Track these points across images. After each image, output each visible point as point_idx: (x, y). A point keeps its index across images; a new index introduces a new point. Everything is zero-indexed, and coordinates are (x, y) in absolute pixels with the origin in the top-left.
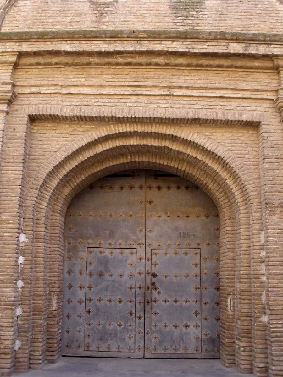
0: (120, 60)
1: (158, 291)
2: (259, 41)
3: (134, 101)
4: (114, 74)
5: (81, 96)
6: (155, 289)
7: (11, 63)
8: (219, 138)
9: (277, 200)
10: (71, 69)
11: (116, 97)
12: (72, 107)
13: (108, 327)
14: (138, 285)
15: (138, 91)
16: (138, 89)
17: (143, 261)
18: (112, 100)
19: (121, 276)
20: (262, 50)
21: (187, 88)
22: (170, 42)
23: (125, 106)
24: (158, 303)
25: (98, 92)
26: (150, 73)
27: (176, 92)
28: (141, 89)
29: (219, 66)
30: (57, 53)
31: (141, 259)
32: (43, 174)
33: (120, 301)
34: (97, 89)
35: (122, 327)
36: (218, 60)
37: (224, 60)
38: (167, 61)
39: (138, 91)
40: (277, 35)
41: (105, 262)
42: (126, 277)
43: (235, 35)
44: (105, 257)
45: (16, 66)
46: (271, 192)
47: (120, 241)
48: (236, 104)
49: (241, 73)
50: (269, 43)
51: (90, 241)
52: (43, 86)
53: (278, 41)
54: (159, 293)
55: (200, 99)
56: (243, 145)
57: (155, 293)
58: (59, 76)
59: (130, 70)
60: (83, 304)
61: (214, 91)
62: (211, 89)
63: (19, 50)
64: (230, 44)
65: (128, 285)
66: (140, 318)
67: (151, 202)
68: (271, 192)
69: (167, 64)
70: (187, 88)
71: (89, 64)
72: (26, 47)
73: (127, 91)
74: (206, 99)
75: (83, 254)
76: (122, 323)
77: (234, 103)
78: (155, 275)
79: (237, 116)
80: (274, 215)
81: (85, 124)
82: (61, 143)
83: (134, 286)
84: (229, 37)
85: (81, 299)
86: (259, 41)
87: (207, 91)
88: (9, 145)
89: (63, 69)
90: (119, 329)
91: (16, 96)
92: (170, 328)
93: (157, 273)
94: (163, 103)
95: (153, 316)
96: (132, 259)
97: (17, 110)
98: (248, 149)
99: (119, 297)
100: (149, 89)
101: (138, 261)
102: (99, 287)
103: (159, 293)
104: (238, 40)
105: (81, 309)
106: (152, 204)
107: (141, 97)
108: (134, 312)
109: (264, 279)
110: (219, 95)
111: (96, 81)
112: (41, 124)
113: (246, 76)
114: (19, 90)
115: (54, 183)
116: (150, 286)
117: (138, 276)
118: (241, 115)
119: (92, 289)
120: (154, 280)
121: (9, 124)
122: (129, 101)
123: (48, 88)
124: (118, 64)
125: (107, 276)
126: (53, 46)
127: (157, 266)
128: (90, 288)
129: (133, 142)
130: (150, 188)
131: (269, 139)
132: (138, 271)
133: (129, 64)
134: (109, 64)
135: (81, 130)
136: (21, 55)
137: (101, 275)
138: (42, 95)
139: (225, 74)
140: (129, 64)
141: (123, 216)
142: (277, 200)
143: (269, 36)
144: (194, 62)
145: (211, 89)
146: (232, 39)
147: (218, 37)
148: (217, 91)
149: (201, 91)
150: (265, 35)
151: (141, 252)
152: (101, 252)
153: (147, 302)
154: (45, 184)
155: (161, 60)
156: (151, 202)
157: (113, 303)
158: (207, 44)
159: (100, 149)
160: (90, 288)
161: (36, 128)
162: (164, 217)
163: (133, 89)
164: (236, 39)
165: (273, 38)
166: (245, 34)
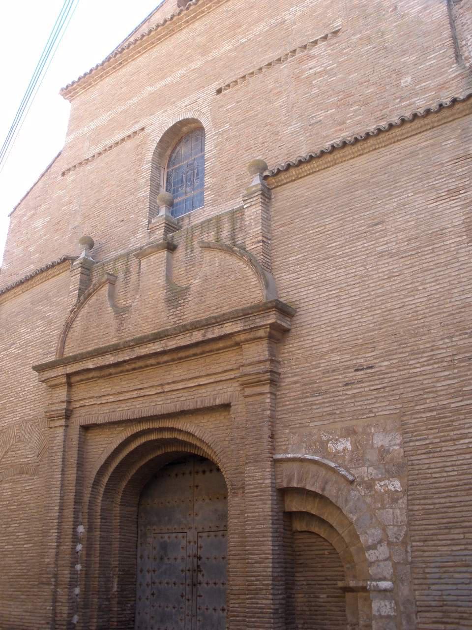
0: (128, 367)
1: (202, 573)
2: (213, 324)
3: (141, 402)
4: (128, 380)
5: (109, 404)
6: (200, 571)
7: (65, 383)
8: (205, 424)
9: (239, 481)
10: (102, 380)
11: (130, 401)
12: (104, 415)
13: (166, 609)
14: (187, 568)
15: (142, 393)
16: (142, 391)
17: (192, 544)
18: (128, 405)
19: (175, 559)
20: (216, 332)
21: (174, 382)
22: (152, 345)
23: (136, 408)
24: (202, 585)
25: (118, 399)
26: (151, 373)
27: (167, 388)
28: (144, 390)
29: (195, 355)
30: (88, 370)
31: (189, 542)
32: (95, 473)
33: (175, 584)
34: (117, 396)
35: (176, 609)
36: (192, 350)
37: (196, 349)
38: (157, 361)
39: (142, 393)
40: (224, 314)
41: (164, 547)
42: (179, 561)
43: (193, 325)
44: (165, 541)
45: (70, 385)
46: (235, 474)
47: (175, 526)
48: (211, 389)
49: (214, 356)
50: (222, 323)
51: (155, 527)
52: (86, 399)
53: (229, 319)
54: (203, 575)
55: (185, 391)
56: (224, 428)
57: (200, 576)
58: (96, 388)
59: (137, 374)
60: (150, 587)
61: (191, 381)
62: (190, 379)
63: (65, 373)
64: (193, 333)
65: (181, 568)
66: (188, 600)
67: (197, 486)
68: (235, 474)
69: (159, 363)
70: (174, 382)
71: (110, 374)
72: (70, 369)
73: (135, 394)
74: (189, 390)
75: (150, 540)
76: (176, 606)
77: (210, 389)
78: (200, 558)
79: (212, 401)
80: (237, 496)
81: (118, 427)
82: (104, 446)
83: (184, 569)
84: (188, 327)
85: (148, 582)
86: (213, 324)
87: (189, 382)
88: (69, 453)
89: (98, 381)
90: (174, 611)
91: (72, 411)
92: (211, 611)
93: (202, 556)
94: (159, 400)
95: (198, 598)
96: (184, 543)
97: (73, 423)
98: (229, 431)
99: (174, 580)
100: (149, 390)
101: (188, 544)
102: (160, 570)
103: (203, 575)
104: (197, 328)
105: (148, 592)
106: (199, 488)
107: (146, 398)
108: (184, 594)
109: (376, 533)
110: (196, 384)
111: (117, 389)
112: (93, 431)
113: (217, 358)
114: (74, 405)
115: (105, 480)
116: (196, 568)
117: (188, 558)
118: (215, 399)
119: (156, 572)
120: (199, 562)
121: (271, 422)
122: (138, 403)
123: (89, 400)
124: (128, 371)
125: (166, 560)
126: (83, 365)
127: (202, 549)
128: (154, 571)
129: (153, 437)
130: (197, 472)
131: (236, 419)
132: (188, 554)
133: (134, 369)
134: (122, 372)
135: (116, 432)
136: (69, 376)
137: (162, 559)
138: (87, 407)
139: (202, 361)
140: (134, 369)
141: (178, 501)
142: (239, 481)
143: (219, 317)
144: (175, 356)
145: (190, 379)
146: (192, 329)
147: (182, 330)
148: (195, 380)
149: (184, 383)
150: (215, 318)
151: (190, 535)
152: (162, 538)
153: (195, 584)
154: (97, 482)
155: (152, 361)
156: (197, 486)
157: (170, 586)
158: (177, 338)
159: (133, 446)
160: (154, 571)
161: (89, 435)
162: (207, 501)
163: (139, 392)
164: (196, 328)
165: (222, 319)
166: (198, 321)
